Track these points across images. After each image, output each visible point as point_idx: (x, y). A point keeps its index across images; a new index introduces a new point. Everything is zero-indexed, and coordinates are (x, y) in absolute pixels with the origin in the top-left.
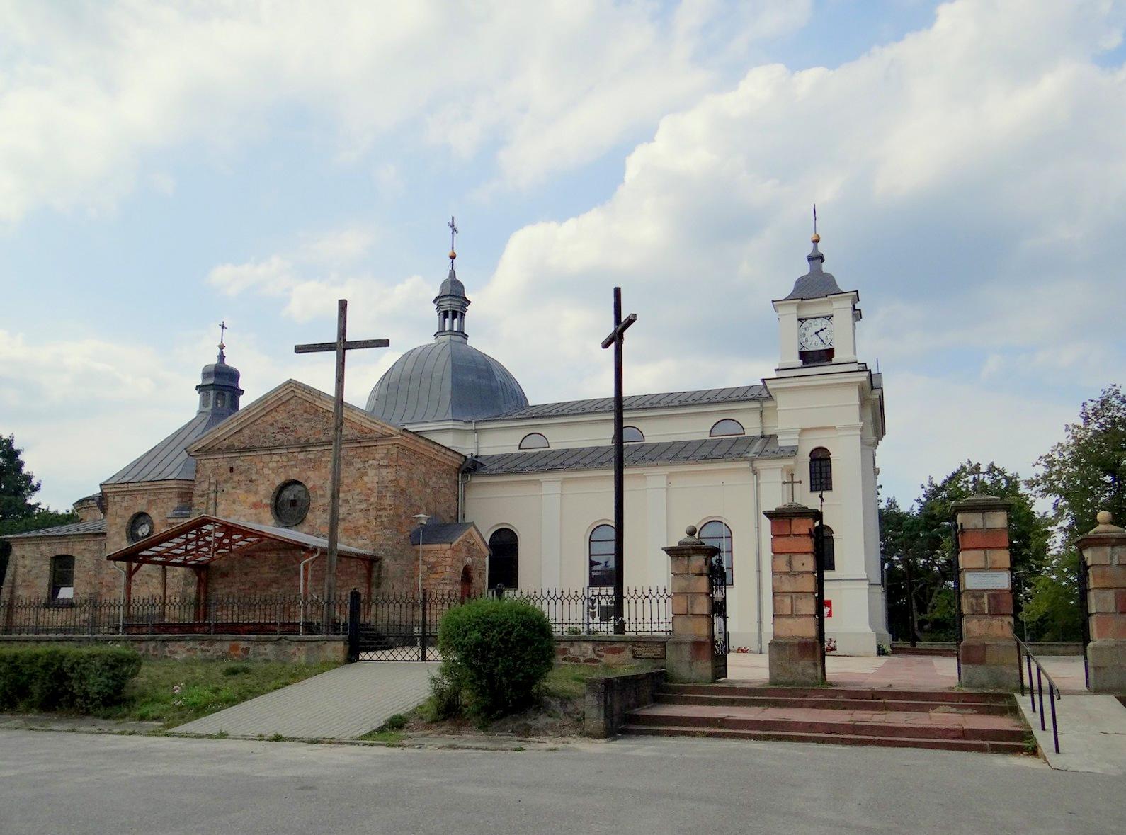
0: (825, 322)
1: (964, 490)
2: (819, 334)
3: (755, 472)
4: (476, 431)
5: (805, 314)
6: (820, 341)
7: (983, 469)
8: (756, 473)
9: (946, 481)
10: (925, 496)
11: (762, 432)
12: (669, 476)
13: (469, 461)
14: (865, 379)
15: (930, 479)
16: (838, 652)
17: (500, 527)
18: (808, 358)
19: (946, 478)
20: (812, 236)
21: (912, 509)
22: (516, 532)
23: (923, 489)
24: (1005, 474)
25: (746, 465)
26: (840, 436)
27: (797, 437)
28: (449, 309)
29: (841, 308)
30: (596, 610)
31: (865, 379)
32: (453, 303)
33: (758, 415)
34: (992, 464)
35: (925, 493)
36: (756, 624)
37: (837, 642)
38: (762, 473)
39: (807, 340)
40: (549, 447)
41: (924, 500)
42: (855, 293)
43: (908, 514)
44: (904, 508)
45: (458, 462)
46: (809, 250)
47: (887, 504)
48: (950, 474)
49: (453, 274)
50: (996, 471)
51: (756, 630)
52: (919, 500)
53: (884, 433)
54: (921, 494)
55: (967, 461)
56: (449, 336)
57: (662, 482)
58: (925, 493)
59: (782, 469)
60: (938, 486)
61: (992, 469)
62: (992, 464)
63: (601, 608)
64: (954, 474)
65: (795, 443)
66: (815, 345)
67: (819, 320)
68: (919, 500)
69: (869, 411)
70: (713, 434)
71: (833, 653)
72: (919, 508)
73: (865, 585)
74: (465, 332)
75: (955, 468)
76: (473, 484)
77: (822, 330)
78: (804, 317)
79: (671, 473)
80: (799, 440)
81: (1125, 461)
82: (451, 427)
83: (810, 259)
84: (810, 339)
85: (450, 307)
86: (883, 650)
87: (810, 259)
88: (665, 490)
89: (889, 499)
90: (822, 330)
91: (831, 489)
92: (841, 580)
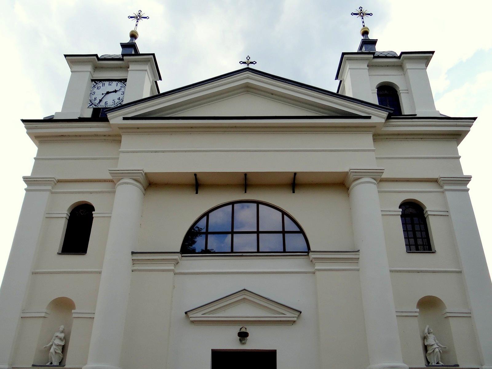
0: (120, 84)
46: (127, 39)
67: (114, 83)
74: (370, 39)
77: (115, 91)
87: (123, 46)
90: (115, 91)
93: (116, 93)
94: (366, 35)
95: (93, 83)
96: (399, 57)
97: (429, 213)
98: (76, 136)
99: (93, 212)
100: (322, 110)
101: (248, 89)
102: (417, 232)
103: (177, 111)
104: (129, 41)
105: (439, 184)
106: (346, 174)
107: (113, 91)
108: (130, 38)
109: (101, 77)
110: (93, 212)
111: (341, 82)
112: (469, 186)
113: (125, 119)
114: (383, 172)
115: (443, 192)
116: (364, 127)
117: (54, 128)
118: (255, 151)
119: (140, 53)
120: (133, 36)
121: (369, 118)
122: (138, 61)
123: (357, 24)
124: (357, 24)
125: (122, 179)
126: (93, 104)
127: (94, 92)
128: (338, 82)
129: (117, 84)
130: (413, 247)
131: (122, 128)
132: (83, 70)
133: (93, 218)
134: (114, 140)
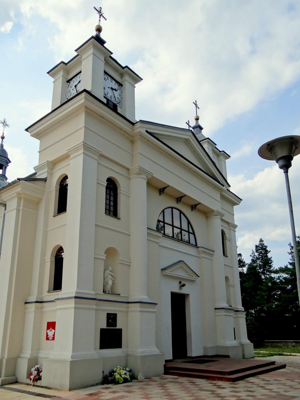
14: (83, 101)
49: (286, 172)
94: (197, 120)
96: (220, 152)
97: (121, 192)
98: (110, 122)
100: (207, 170)
101: (187, 142)
102: (109, 199)
103: (163, 138)
105: (129, 172)
106: (213, 211)
109: (114, 77)
111: (78, 55)
112: (236, 230)
113: (147, 131)
114: (224, 216)
115: (229, 229)
116: (199, 175)
117: (236, 200)
120: (99, 30)
121: (223, 186)
122: (133, 78)
123: (95, 20)
124: (95, 20)
125: (142, 174)
128: (76, 54)
130: (112, 213)
131: (141, 135)
132: (98, 56)
134: (128, 138)
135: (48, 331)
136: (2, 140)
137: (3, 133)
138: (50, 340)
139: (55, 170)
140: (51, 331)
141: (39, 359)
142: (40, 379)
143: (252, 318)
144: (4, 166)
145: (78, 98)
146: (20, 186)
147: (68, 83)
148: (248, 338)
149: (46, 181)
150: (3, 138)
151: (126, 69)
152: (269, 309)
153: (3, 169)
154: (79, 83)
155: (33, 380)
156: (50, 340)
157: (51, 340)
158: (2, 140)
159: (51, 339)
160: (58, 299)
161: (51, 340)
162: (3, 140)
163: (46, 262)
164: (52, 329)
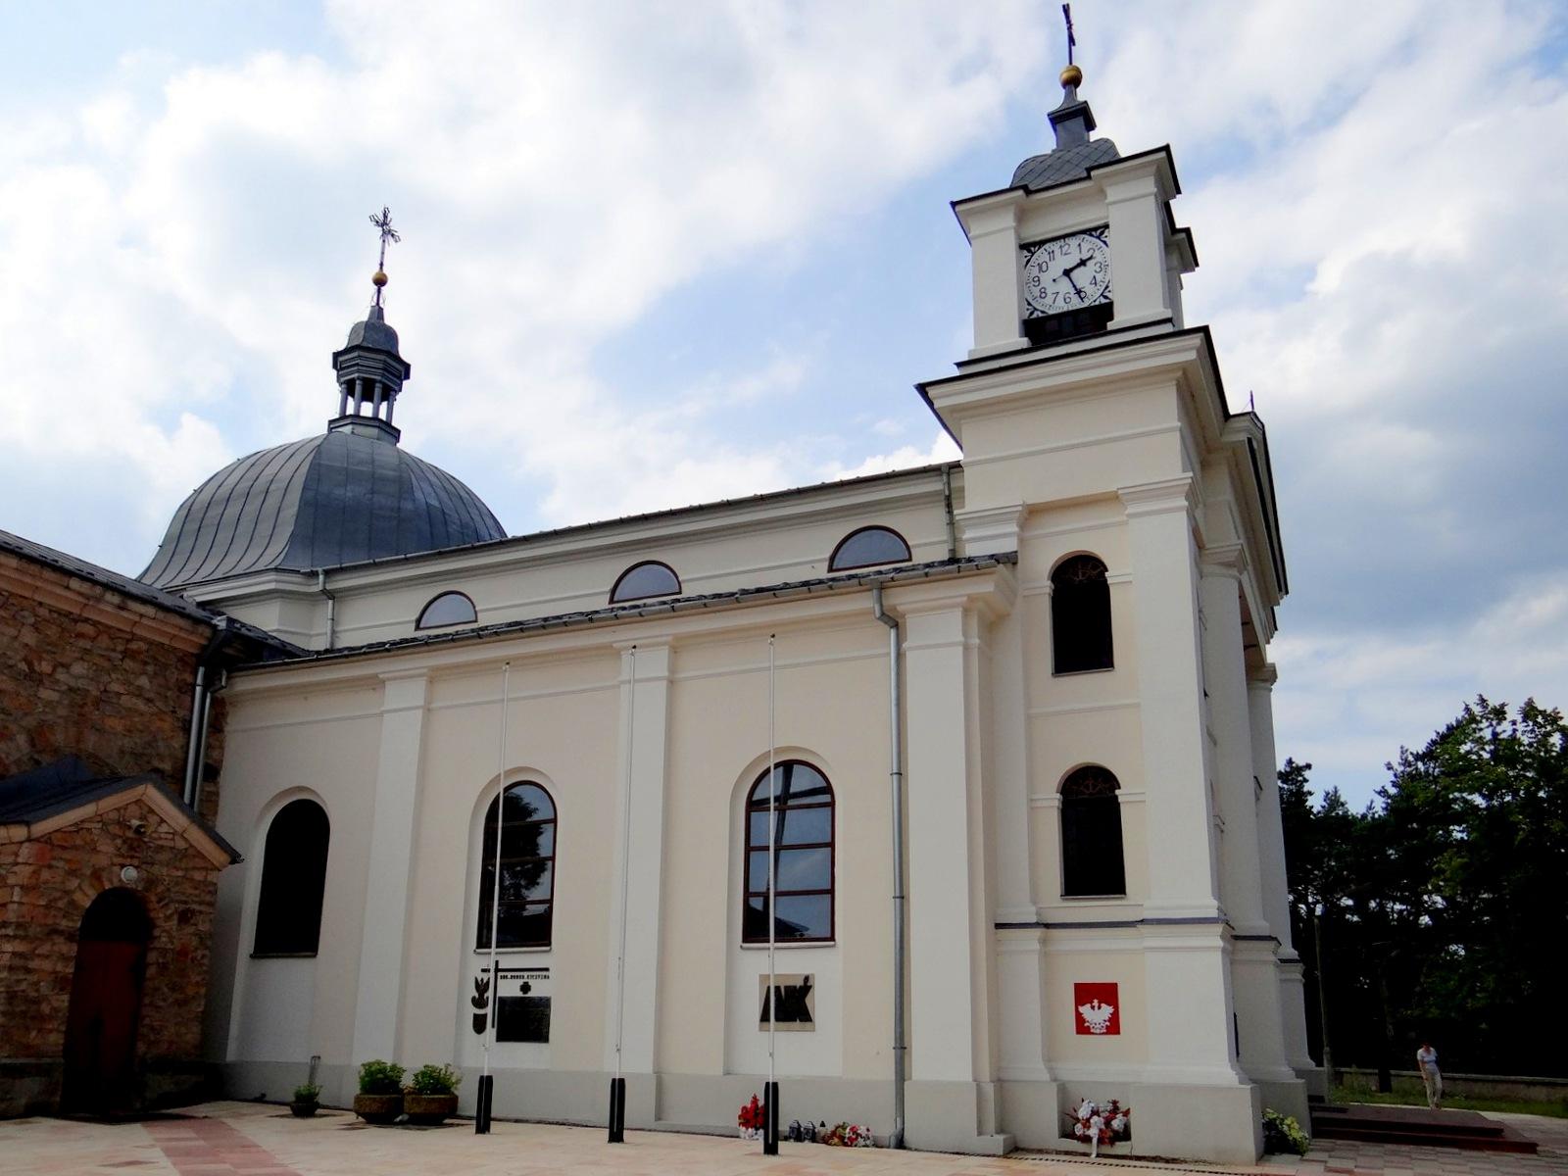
0: (1089, 242)
1: (1474, 757)
2: (1074, 275)
3: (893, 621)
4: (330, 595)
5: (1036, 231)
6: (1073, 291)
7: (1513, 713)
8: (896, 625)
9: (1434, 742)
10: (1394, 784)
11: (953, 551)
12: (676, 649)
13: (222, 634)
14: (1192, 355)
15: (1402, 753)
16: (1138, 1144)
17: (294, 799)
18: (1043, 331)
19: (1434, 736)
20: (1061, 71)
21: (1370, 808)
22: (322, 805)
23: (1391, 772)
24: (1561, 723)
25: (866, 602)
26: (1130, 516)
27: (1014, 528)
28: (356, 375)
29: (1129, 211)
30: (489, 1010)
31: (1192, 355)
32: (373, 365)
33: (941, 512)
34: (1530, 704)
35: (1393, 779)
36: (890, 1055)
37: (1132, 1116)
38: (911, 624)
39: (1043, 293)
40: (476, 621)
41: (1393, 791)
42: (1163, 154)
43: (1364, 816)
44: (1356, 807)
45: (192, 641)
46: (1056, 99)
47: (1324, 804)
48: (1443, 729)
49: (378, 312)
50: (1540, 717)
51: (888, 1073)
52: (1383, 792)
53: (1283, 587)
54: (1386, 780)
55: (1476, 699)
56: (350, 427)
57: (655, 663)
58: (1393, 779)
59: (966, 612)
60: (1421, 752)
61: (1530, 712)
62: (1530, 704)
63: (503, 1003)
64: (1450, 728)
65: (1007, 546)
66: (1059, 300)
67: (1073, 242)
68: (1383, 792)
69: (1223, 493)
70: (837, 564)
71: (1121, 1148)
72: (1384, 805)
73: (1213, 939)
74: (393, 424)
75: (1453, 714)
76: (243, 693)
77: (1083, 263)
78: (1038, 239)
79: (678, 638)
80: (1022, 541)
81: (1453, 947)
82: (272, 586)
83: (1057, 119)
84: (1051, 289)
85: (358, 371)
86: (1284, 1136)
87: (1057, 119)
88: (665, 683)
89: (1328, 794)
90: (1083, 263)
91: (1112, 666)
92: (1142, 921)
93: (1085, 265)
95: (1025, 253)
99: (1117, 792)
104: (1274, 696)
107: (1075, 264)
108: (1062, 92)
110: (1117, 792)
118: (401, 710)
119: (1123, 154)
126: (1036, 309)
127: (1036, 279)
129: (1079, 245)
133: (1119, 804)
135: (1085, 1010)
136: (379, 292)
137: (382, 265)
138: (1096, 1034)
139: (1036, 533)
140: (1096, 1008)
141: (1067, 1086)
142: (1125, 1135)
143: (1464, 993)
144: (378, 385)
145: (1171, 343)
146: (994, 577)
147: (1025, 251)
148: (1310, 1054)
149: (1015, 563)
150: (380, 282)
151: (1183, 235)
152: (164, 939)
153: (356, 396)
154: (1078, 266)
155: (1101, 1141)
156: (1096, 1034)
157: (1100, 1034)
158: (379, 292)
159: (1098, 1031)
160: (1142, 921)
161: (1100, 1034)
162: (382, 288)
163: (1037, 807)
164: (1100, 1003)
